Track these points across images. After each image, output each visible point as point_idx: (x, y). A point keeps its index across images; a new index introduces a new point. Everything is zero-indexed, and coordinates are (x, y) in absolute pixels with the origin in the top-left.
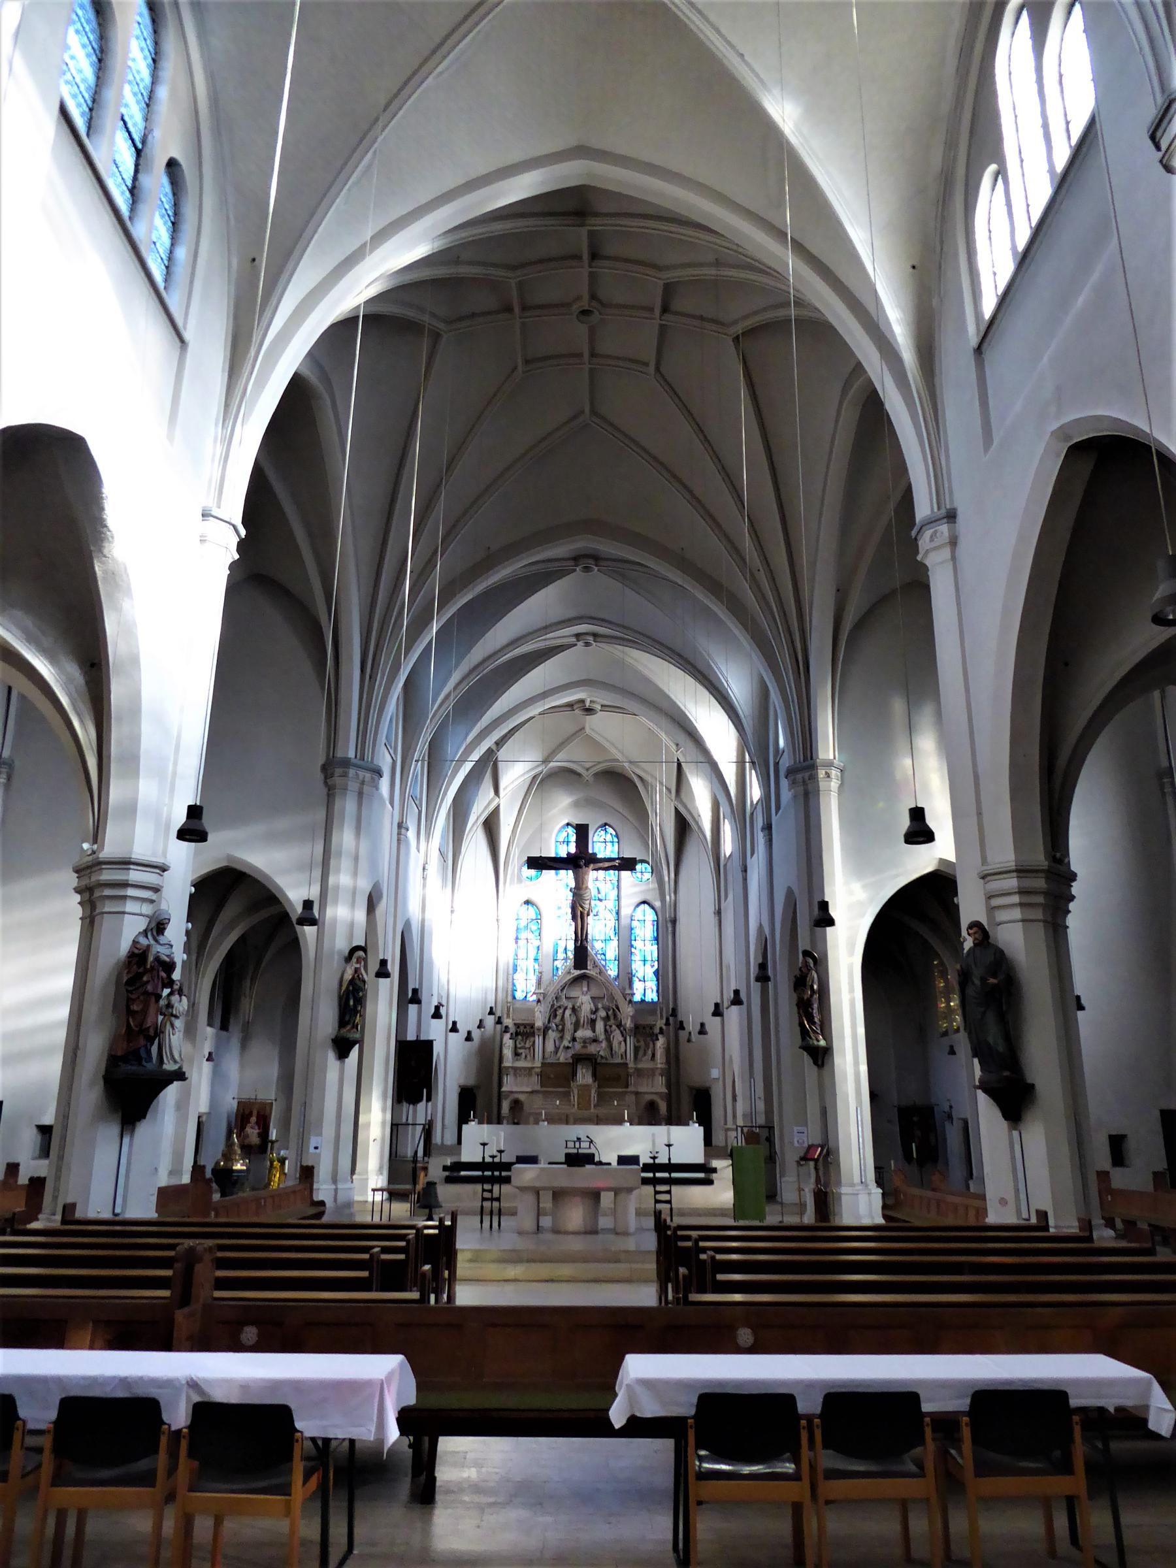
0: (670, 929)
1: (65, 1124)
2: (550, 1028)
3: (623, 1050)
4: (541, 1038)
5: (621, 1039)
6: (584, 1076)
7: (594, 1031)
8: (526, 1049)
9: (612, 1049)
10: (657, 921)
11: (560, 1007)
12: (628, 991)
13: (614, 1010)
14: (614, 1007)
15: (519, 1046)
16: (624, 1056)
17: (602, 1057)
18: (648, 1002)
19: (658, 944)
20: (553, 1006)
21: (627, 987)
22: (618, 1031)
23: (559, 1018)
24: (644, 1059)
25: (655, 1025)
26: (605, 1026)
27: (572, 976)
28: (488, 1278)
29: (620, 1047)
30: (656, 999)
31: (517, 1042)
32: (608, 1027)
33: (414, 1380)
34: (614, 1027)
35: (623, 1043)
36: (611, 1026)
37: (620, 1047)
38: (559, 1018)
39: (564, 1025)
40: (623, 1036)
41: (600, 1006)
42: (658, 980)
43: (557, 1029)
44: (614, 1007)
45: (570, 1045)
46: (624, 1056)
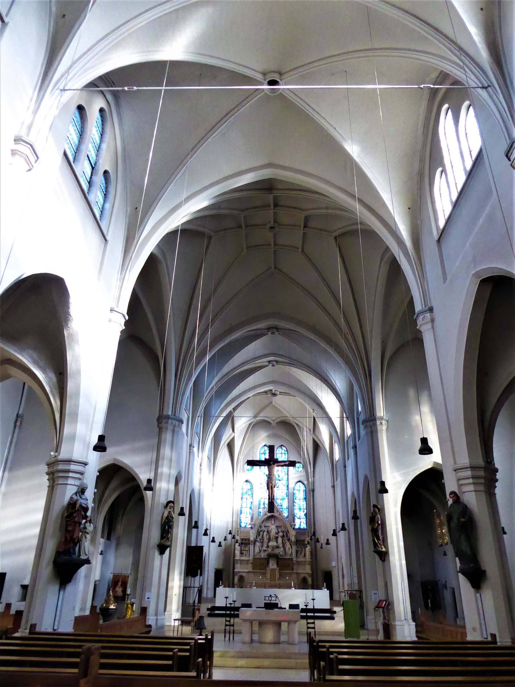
3: (291, 552)
5: (290, 546)
7: (277, 543)
8: (245, 551)
9: (285, 552)
10: (306, 490)
11: (261, 531)
12: (293, 524)
15: (242, 549)
18: (302, 529)
20: (258, 530)
23: (261, 536)
26: (283, 540)
29: (289, 551)
34: (286, 541)
35: (291, 549)
39: (263, 539)
41: (280, 530)
42: (306, 518)
45: (266, 549)
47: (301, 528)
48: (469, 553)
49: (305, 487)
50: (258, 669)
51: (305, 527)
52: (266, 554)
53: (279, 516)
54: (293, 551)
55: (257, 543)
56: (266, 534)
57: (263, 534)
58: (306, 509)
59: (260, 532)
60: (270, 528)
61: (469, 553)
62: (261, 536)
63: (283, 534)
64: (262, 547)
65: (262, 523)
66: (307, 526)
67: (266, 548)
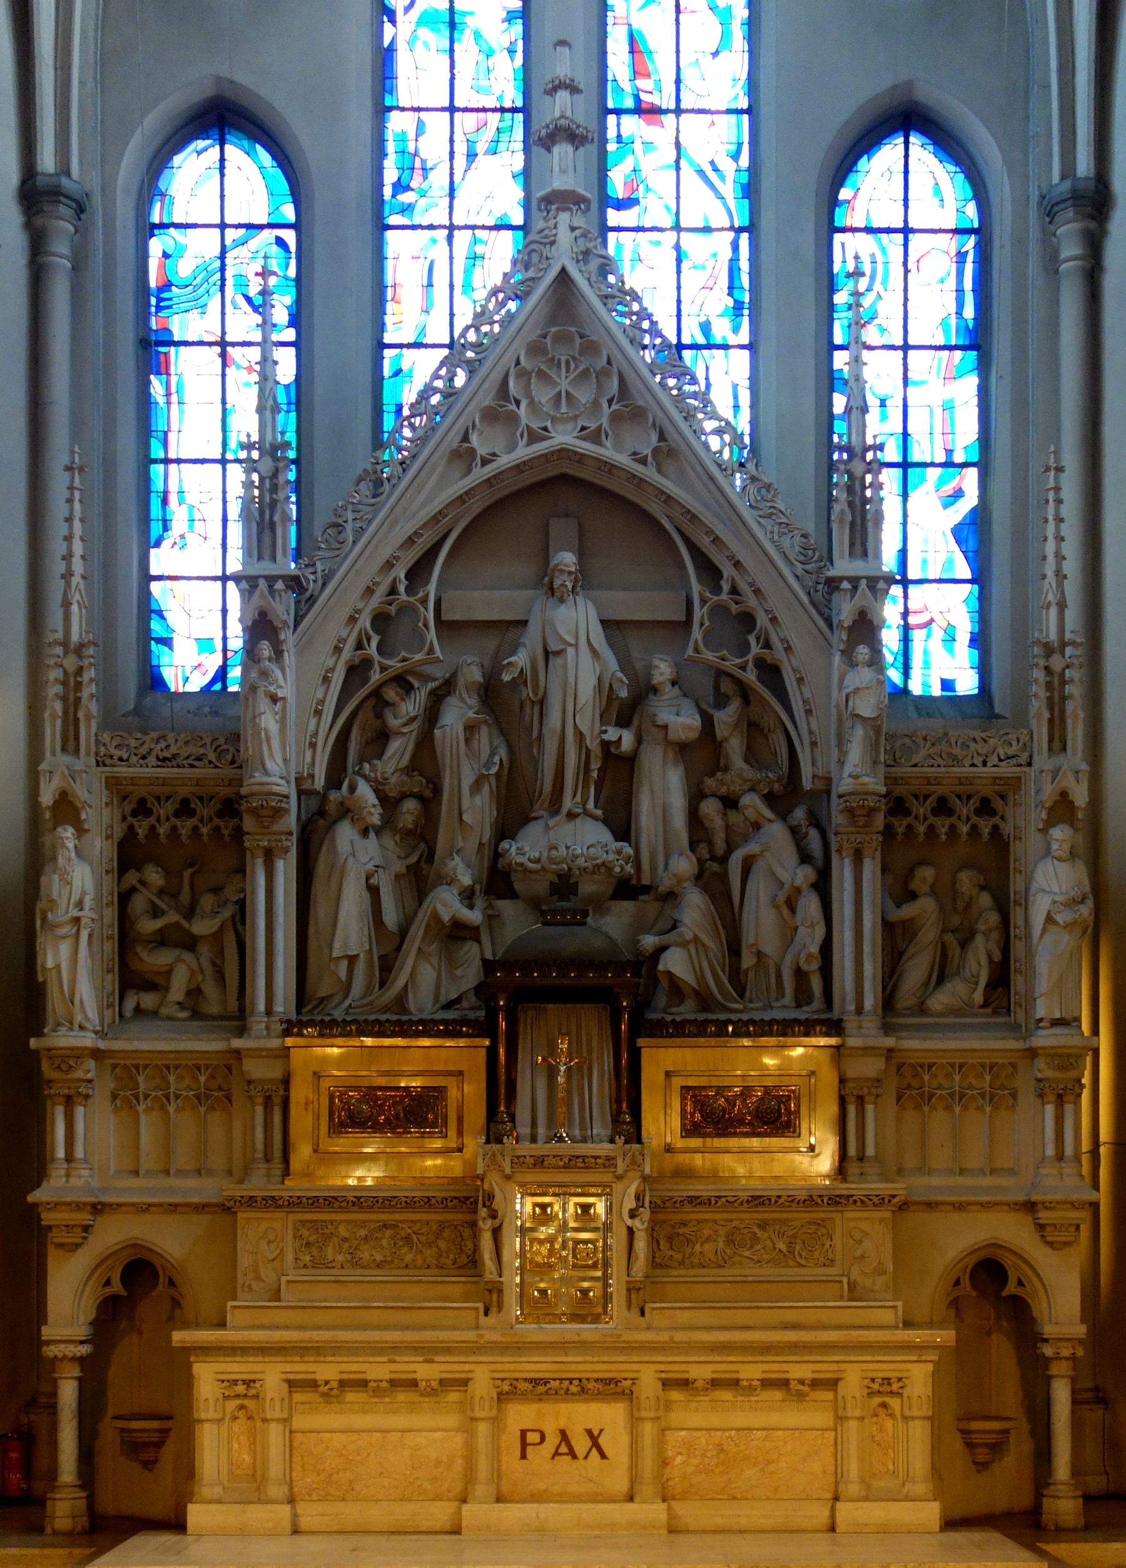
0: (1071, 249)
1: (860, 1052)
2: (346, 811)
3: (810, 940)
4: (286, 870)
5: (804, 875)
6: (603, 870)
7: (623, 830)
8: (190, 943)
9: (734, 948)
10: (982, 232)
11: (403, 682)
12: (843, 566)
13: (745, 692)
14: (751, 676)
15: (148, 926)
16: (816, 983)
17: (676, 989)
18: (925, 701)
19: (983, 368)
20: (357, 671)
21: (841, 538)
22: (776, 833)
23: (399, 751)
24: (939, 1000)
25: (1016, 783)
26: (696, 796)
27: (480, 474)
28: (373, 1529)
29: (789, 934)
30: (967, 684)
31: (139, 903)
32: (710, 808)
33: (884, 508)
34: (752, 802)
35: (810, 905)
36: (730, 803)
37: (789, 934)
38: (399, 751)
39: (430, 801)
40: (805, 858)
41: (663, 671)
42: (980, 578)
43: (388, 823)
44: (751, 676)
45: (474, 916)
46: (816, 983)
47: (916, 688)
48: (344, 979)
49: (980, 194)
50: (910, 204)
51: (967, 684)
52: (470, 975)
53: (649, 473)
54: (844, 939)
55: (345, 834)
56: (471, 729)
57: (432, 715)
58: (984, 466)
59: (378, 701)
60: (532, 638)
61: (344, 979)
62: (394, 745)
63: (708, 722)
64: (421, 895)
65: (418, 573)
66: (984, 669)
67: (468, 896)
